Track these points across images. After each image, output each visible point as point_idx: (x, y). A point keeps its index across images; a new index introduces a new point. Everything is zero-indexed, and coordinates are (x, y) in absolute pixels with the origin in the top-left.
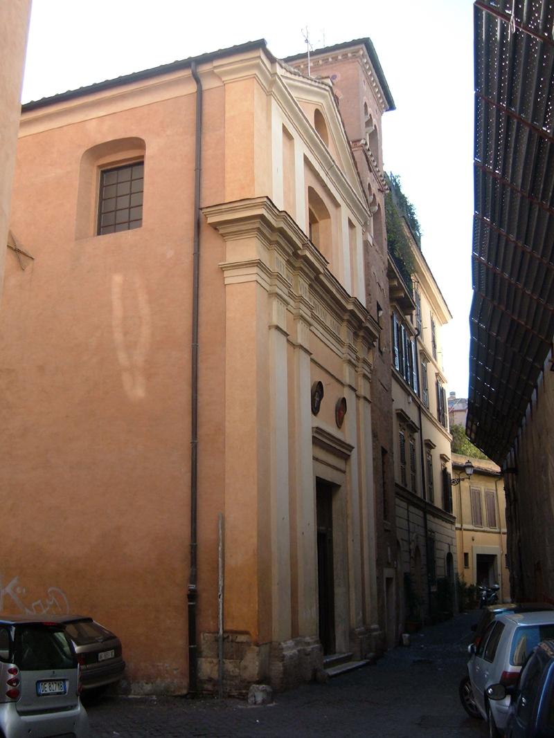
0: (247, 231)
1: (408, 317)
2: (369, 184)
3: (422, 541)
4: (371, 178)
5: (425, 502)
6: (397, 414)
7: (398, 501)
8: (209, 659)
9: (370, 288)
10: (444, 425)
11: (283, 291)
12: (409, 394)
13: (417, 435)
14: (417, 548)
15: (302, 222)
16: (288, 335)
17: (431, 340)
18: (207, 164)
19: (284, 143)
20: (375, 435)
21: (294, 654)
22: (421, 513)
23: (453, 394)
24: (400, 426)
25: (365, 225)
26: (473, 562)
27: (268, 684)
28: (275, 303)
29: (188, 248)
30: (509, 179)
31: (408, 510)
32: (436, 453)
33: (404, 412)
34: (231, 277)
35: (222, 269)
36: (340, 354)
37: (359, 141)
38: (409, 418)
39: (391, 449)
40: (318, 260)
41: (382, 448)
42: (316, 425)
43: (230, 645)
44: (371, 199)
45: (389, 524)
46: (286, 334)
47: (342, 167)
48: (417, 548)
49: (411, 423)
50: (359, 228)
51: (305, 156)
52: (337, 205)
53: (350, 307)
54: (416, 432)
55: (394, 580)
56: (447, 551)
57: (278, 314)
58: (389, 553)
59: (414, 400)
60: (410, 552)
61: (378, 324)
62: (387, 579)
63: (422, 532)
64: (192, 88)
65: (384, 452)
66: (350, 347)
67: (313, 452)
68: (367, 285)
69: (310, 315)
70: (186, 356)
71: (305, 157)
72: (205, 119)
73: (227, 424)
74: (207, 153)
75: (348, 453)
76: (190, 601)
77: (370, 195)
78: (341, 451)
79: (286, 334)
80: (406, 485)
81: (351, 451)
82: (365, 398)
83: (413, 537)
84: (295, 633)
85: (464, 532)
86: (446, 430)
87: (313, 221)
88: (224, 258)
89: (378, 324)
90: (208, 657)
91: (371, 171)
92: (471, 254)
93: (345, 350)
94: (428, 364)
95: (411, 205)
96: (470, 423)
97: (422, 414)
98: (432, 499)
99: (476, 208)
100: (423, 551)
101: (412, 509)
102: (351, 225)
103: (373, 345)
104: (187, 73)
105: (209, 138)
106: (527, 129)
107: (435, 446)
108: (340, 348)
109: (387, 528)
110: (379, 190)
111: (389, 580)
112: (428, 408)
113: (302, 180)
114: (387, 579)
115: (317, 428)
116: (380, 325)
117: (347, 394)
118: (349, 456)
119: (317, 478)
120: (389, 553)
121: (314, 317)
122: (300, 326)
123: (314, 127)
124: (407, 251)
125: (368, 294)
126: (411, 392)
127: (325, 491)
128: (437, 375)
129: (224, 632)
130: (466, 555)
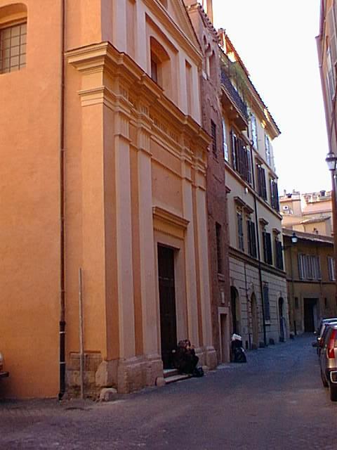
1: (245, 132)
2: (205, 37)
3: (257, 289)
4: (206, 31)
6: (260, 222)
7: (231, 259)
8: (75, 372)
10: (265, 198)
11: (127, 112)
13: (252, 215)
14: (253, 293)
15: (143, 61)
19: (127, 3)
20: (209, 214)
21: (137, 367)
22: (257, 270)
23: (332, 235)
24: (238, 208)
25: (200, 66)
26: (301, 304)
27: (116, 388)
31: (245, 267)
39: (226, 225)
40: (137, 71)
41: (216, 223)
43: (88, 363)
44: (205, 47)
45: (223, 276)
46: (128, 141)
47: (180, 25)
48: (253, 293)
50: (194, 68)
52: (176, 51)
54: (251, 213)
55: (228, 316)
56: (279, 296)
57: (121, 127)
58: (223, 296)
60: (247, 297)
61: (156, 83)
62: (221, 315)
63: (257, 282)
65: (218, 226)
67: (154, 224)
68: (202, 108)
71: (186, 61)
76: (61, 331)
77: (205, 43)
78: (181, 225)
79: (128, 141)
80: (243, 250)
81: (187, 224)
82: (187, 179)
83: (249, 286)
84: (139, 350)
85: (295, 284)
87: (155, 64)
89: (156, 83)
90: (73, 370)
91: (205, 27)
97: (257, 201)
100: (258, 296)
101: (248, 266)
102: (188, 65)
103: (208, 150)
109: (221, 279)
110: (213, 40)
111: (223, 316)
113: (143, 34)
114: (221, 315)
115: (156, 207)
116: (159, 83)
118: (186, 228)
119: (158, 243)
120: (223, 296)
121: (153, 129)
122: (141, 136)
125: (203, 114)
127: (167, 257)
128: (270, 174)
129: (84, 352)
130: (296, 299)
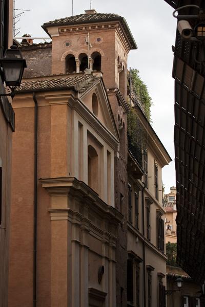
0: (62, 193)
5: (195, 70)
9: (117, 168)
12: (136, 236)
13: (141, 264)
16: (88, 248)
17: (154, 183)
18: (41, 151)
20: (117, 282)
28: (74, 229)
29: (31, 198)
30: (191, 192)
32: (154, 274)
33: (134, 253)
34: (54, 217)
35: (50, 212)
36: (100, 239)
37: (114, 89)
38: (136, 255)
42: (90, 287)
49: (137, 258)
51: (88, 130)
52: (101, 146)
53: (108, 211)
59: (140, 239)
64: (32, 104)
66: (107, 234)
69: (88, 225)
70: (30, 256)
72: (39, 124)
73: (52, 292)
74: (42, 144)
75: (104, 297)
86: (163, 253)
88: (50, 206)
92: (174, 103)
93: (104, 236)
94: (151, 205)
95: (150, 98)
96: (179, 258)
98: (149, 240)
99: (176, 100)
104: (31, 96)
105: (42, 136)
106: (191, 185)
107: (154, 269)
108: (100, 235)
112: (150, 240)
115: (92, 289)
117: (104, 263)
123: (92, 112)
124: (141, 85)
126: (137, 233)
